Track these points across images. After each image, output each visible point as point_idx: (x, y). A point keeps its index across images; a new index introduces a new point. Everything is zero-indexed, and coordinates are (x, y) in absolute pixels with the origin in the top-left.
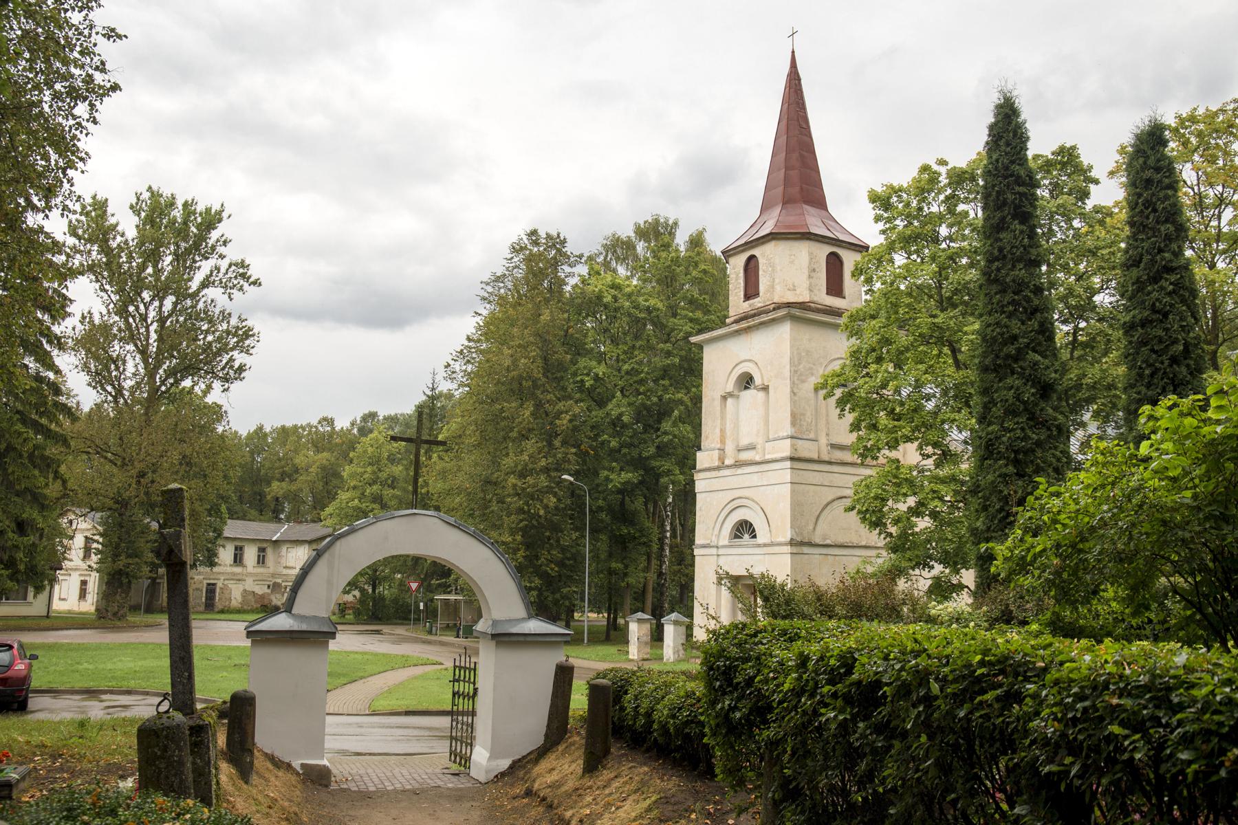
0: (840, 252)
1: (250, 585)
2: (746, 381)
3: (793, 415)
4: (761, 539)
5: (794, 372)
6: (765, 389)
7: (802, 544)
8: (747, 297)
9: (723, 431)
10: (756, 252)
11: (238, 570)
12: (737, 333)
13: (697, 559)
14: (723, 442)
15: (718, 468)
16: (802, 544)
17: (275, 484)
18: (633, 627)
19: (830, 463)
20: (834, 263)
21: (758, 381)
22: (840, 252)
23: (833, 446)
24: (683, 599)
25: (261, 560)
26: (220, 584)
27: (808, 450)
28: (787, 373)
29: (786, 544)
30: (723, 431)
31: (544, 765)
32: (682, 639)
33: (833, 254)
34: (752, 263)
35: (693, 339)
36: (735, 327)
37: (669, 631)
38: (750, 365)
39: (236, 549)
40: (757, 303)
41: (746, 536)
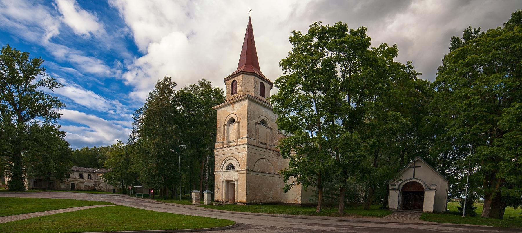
0: (264, 83)
1: (86, 184)
2: (232, 121)
3: (248, 131)
4: (237, 169)
5: (249, 117)
6: (238, 122)
7: (250, 171)
8: (232, 94)
9: (224, 137)
10: (236, 79)
11: (82, 180)
12: (229, 105)
13: (215, 176)
14: (224, 140)
15: (222, 148)
16: (250, 171)
17: (100, 160)
18: (193, 194)
19: (260, 147)
20: (262, 86)
21: (236, 120)
22: (264, 83)
23: (261, 143)
24: (211, 187)
25: (90, 177)
26: (76, 183)
27: (253, 142)
28: (246, 117)
29: (245, 170)
30: (224, 137)
31: (216, 194)
32: (210, 198)
33: (261, 83)
34: (234, 83)
35: (214, 108)
36: (228, 103)
37: (206, 195)
38: (233, 115)
39: (89, 175)
40: (236, 95)
41: (232, 169)
